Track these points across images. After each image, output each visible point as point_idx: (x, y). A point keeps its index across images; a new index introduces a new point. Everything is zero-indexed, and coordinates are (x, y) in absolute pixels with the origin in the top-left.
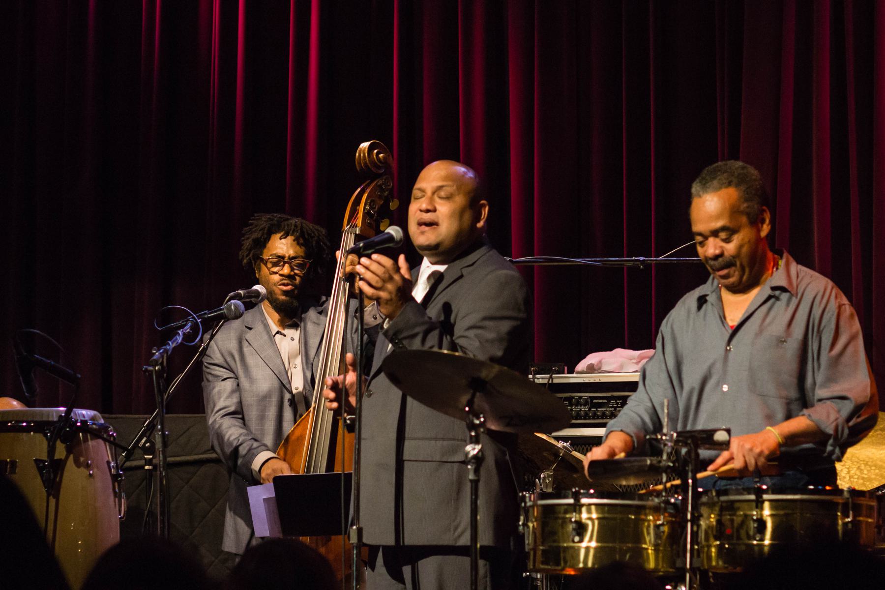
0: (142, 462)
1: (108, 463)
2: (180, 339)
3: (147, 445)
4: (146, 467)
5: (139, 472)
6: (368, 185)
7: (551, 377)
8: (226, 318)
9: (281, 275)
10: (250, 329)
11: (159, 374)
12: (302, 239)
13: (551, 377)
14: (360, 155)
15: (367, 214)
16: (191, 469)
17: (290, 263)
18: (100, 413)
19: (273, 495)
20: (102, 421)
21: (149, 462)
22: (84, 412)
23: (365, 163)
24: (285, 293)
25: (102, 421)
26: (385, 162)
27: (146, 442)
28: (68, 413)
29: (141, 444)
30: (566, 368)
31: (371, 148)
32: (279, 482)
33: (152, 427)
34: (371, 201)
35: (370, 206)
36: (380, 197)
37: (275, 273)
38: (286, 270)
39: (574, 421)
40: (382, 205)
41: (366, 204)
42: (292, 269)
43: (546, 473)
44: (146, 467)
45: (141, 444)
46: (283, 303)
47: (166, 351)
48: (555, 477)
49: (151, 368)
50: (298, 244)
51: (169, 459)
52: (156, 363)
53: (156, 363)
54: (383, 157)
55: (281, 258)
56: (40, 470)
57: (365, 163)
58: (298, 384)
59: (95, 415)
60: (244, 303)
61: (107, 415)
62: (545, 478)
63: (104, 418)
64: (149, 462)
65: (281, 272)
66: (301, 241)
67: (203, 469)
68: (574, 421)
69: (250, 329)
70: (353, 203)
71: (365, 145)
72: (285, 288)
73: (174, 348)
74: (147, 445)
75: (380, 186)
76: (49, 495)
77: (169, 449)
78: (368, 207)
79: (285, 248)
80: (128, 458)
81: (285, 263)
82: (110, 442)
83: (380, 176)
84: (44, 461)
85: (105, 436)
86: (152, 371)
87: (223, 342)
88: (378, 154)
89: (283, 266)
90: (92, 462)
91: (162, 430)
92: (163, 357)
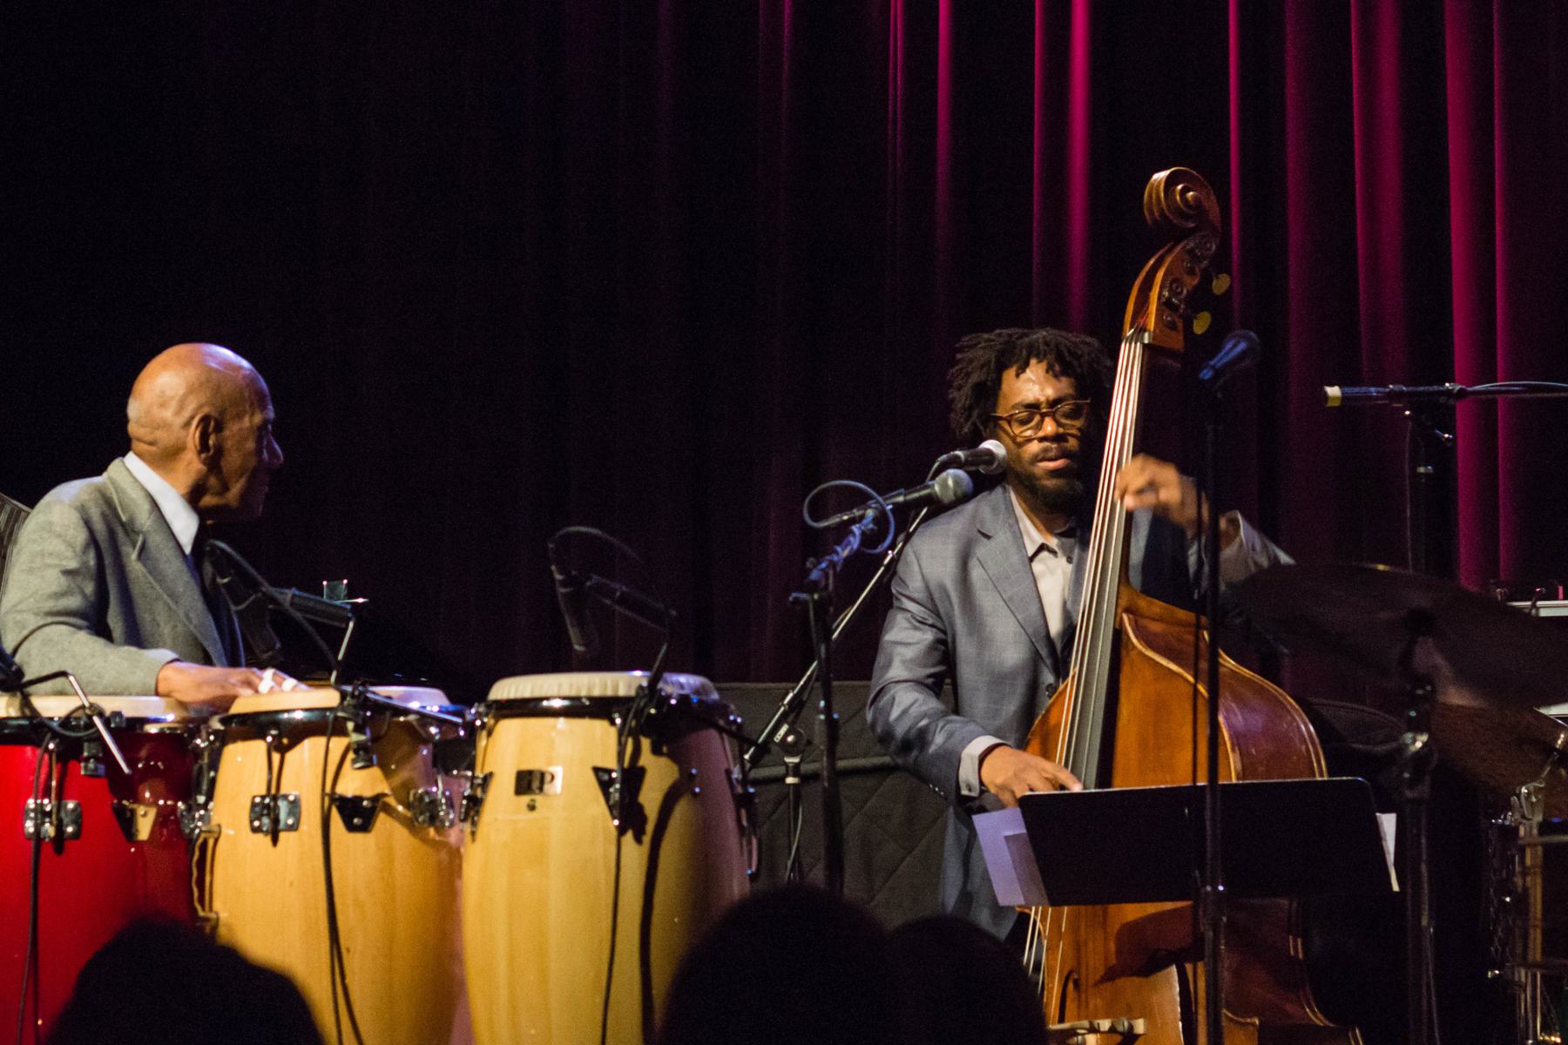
0: (781, 770)
1: (728, 773)
2: (855, 542)
3: (790, 739)
4: (790, 780)
5: (774, 787)
6: (1169, 251)
7: (1534, 606)
8: (938, 508)
9: (1041, 440)
10: (988, 537)
11: (821, 606)
12: (1061, 365)
13: (1534, 606)
14: (1150, 196)
15: (1166, 305)
16: (870, 782)
17: (1053, 415)
18: (712, 679)
19: (1021, 830)
20: (715, 696)
21: (796, 771)
22: (683, 679)
23: (1161, 211)
24: (1054, 473)
25: (715, 696)
26: (1198, 205)
27: (787, 734)
28: (654, 682)
29: (778, 738)
30: (1561, 589)
31: (1170, 182)
32: (1031, 806)
33: (797, 704)
34: (1172, 282)
35: (1170, 290)
36: (1191, 272)
37: (1029, 440)
38: (1049, 427)
39: (743, 812)
40: (1196, 288)
41: (1162, 288)
42: (1059, 424)
43: (1532, 785)
44: (790, 780)
45: (778, 738)
46: (1058, 493)
47: (832, 564)
48: (1548, 792)
49: (804, 596)
50: (1056, 376)
51: (841, 764)
52: (813, 587)
53: (813, 587)
54: (1194, 197)
55: (1033, 407)
56: (605, 786)
57: (1161, 211)
58: (1055, 626)
59: (703, 686)
60: (968, 472)
61: (724, 685)
62: (1529, 794)
63: (719, 690)
64: (796, 771)
65: (1041, 434)
66: (1057, 368)
67: (890, 782)
68: (743, 812)
69: (988, 537)
70: (1140, 290)
71: (1160, 176)
72: (1052, 465)
73: (847, 560)
74: (790, 739)
75: (1191, 252)
76: (621, 831)
77: (841, 747)
78: (1166, 294)
79: (1036, 388)
80: (755, 761)
81: (1043, 416)
82: (731, 734)
83: (1187, 234)
84: (609, 771)
85: (721, 722)
86: (806, 602)
87: (929, 557)
88: (1184, 192)
89: (1042, 421)
90: (700, 772)
91: (828, 710)
92: (827, 576)
